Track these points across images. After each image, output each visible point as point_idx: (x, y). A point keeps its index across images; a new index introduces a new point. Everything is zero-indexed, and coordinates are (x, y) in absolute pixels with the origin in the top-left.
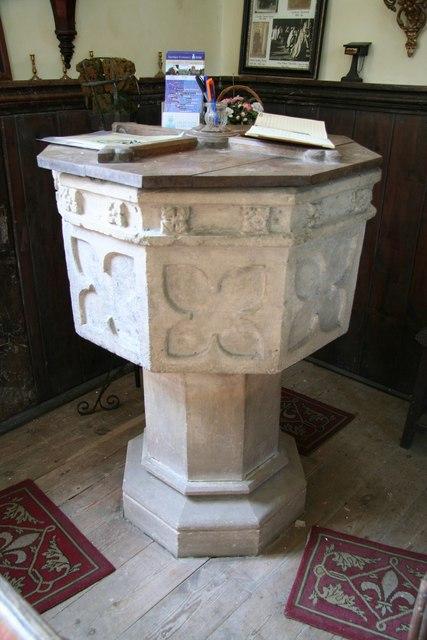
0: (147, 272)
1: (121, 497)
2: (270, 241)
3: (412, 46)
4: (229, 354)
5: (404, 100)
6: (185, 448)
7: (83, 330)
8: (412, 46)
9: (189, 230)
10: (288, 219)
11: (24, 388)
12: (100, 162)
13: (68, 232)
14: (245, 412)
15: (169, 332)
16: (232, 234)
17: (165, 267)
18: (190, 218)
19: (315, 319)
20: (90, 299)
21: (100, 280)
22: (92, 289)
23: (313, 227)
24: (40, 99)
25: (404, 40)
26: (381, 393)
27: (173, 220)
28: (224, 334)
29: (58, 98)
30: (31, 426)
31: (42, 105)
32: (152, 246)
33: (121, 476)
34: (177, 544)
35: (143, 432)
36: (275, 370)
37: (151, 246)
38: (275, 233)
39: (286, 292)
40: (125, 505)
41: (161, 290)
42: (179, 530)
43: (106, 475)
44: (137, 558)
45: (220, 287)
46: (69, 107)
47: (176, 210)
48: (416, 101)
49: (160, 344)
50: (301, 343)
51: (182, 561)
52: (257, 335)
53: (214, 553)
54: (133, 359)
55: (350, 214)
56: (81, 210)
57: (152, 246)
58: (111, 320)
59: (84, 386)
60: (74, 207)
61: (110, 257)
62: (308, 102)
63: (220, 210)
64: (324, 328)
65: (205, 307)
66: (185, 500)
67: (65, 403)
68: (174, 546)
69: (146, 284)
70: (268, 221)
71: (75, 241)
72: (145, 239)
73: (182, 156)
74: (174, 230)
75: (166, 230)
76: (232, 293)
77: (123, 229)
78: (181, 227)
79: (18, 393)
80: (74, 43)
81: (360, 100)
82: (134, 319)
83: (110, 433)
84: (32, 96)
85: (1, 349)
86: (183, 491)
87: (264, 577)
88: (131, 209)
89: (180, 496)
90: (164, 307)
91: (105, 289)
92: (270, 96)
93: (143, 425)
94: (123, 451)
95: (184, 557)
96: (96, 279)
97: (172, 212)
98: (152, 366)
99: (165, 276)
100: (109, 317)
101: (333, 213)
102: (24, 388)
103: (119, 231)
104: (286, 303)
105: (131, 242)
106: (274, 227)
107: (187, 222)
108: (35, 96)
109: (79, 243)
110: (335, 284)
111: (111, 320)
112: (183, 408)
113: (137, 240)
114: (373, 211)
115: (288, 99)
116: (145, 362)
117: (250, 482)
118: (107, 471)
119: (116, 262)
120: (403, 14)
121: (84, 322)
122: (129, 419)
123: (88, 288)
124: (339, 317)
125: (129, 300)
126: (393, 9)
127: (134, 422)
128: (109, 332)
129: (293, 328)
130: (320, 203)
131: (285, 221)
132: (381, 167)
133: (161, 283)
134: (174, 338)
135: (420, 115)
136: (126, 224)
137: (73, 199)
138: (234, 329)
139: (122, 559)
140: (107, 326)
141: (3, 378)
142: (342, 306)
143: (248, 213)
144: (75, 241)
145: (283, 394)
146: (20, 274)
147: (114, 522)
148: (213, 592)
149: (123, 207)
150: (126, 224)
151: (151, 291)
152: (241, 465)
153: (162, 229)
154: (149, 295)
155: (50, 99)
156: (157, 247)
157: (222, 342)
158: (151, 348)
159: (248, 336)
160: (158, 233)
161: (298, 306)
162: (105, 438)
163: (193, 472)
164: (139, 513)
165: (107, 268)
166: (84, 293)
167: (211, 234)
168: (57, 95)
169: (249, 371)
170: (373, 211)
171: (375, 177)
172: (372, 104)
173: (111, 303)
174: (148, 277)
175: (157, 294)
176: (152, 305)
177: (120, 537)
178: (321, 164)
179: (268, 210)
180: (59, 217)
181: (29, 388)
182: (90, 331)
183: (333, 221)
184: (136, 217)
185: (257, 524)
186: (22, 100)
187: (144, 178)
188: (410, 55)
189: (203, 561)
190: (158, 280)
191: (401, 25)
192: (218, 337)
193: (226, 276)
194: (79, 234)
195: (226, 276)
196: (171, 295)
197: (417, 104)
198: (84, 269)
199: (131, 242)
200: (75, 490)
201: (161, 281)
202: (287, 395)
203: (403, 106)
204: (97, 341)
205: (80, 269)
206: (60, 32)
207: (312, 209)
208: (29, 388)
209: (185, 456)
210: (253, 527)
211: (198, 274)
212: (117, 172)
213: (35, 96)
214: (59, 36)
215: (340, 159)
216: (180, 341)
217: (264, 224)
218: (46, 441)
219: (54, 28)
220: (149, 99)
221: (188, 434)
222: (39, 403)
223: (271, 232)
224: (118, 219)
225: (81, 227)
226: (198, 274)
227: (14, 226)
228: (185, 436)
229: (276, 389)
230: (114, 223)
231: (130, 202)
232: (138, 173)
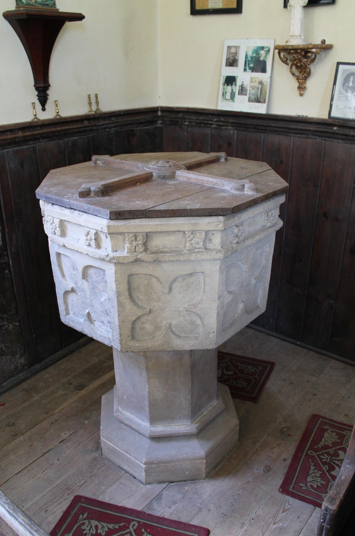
0: (116, 281)
1: (100, 439)
2: (206, 256)
3: (302, 88)
4: (179, 336)
5: (299, 127)
6: (147, 403)
7: (65, 319)
8: (302, 88)
9: (146, 250)
10: (219, 239)
11: (18, 356)
12: (105, 270)
13: (53, 249)
14: (192, 374)
15: (134, 323)
16: (178, 252)
17: (130, 276)
18: (146, 241)
19: (241, 306)
20: (72, 298)
21: (80, 284)
22: (73, 290)
23: (237, 243)
24: (24, 137)
25: (297, 84)
26: (292, 345)
27: (134, 244)
28: (174, 322)
29: (37, 134)
30: (25, 385)
31: (25, 140)
32: (118, 263)
33: (98, 424)
34: (144, 474)
35: (113, 388)
36: (213, 346)
37: (119, 263)
38: (209, 249)
39: (219, 291)
40: (102, 445)
41: (127, 294)
42: (145, 464)
43: (86, 422)
44: (114, 486)
45: (170, 289)
46: (45, 140)
47: (136, 237)
48: (308, 128)
49: (127, 331)
50: (232, 325)
51: (148, 486)
52: (199, 322)
53: (173, 480)
54: (107, 342)
55: (264, 229)
56: (63, 234)
57: (118, 263)
58: (89, 314)
59: (61, 353)
60: (58, 231)
61: (87, 268)
62: (228, 126)
63: (168, 235)
64: (247, 311)
65: (160, 304)
66: (149, 441)
67: (49, 366)
68: (142, 476)
69: (115, 289)
70: (204, 242)
71: (58, 255)
72: (114, 258)
73: (140, 188)
74: (135, 251)
75: (130, 251)
76: (180, 293)
77: (97, 251)
78: (140, 248)
79: (13, 360)
80: (48, 92)
81: (267, 126)
82: (107, 313)
83: (87, 388)
84: (17, 135)
85: (1, 326)
86: (147, 435)
87: (210, 495)
88: (103, 236)
89: (145, 438)
90: (128, 305)
91: (83, 290)
92: (197, 121)
93: (112, 382)
94: (98, 403)
95: (150, 484)
96: (76, 283)
97: (133, 238)
98: (122, 348)
99: (129, 283)
100: (87, 311)
101: (251, 229)
102: (18, 356)
103: (93, 250)
104: (219, 298)
105: (103, 260)
106: (209, 245)
107: (145, 244)
108: (20, 134)
109: (62, 257)
110: (255, 279)
111: (89, 314)
112: (144, 374)
113: (108, 259)
114: (280, 224)
115: (212, 124)
116: (116, 345)
117: (197, 425)
118: (86, 418)
119: (91, 272)
120: (294, 68)
121: (68, 314)
122: (100, 376)
123: (70, 289)
124: (259, 302)
125: (102, 299)
126: (287, 64)
127: (105, 378)
128: (88, 322)
129: (225, 315)
130: (242, 224)
131: (217, 240)
132: (286, 193)
133: (127, 288)
134: (138, 326)
135: (311, 138)
136: (98, 246)
137: (58, 225)
138: (182, 318)
139: (103, 488)
140: (86, 318)
141: (1, 349)
142: (260, 293)
143: (189, 237)
144: (58, 255)
145: (218, 356)
146: (12, 269)
147: (95, 459)
148: (173, 508)
149: (96, 234)
150: (98, 246)
151: (119, 294)
152: (190, 413)
153: (126, 251)
154: (117, 298)
155: (31, 136)
156: (122, 264)
157: (174, 329)
158: (121, 335)
159: (193, 323)
160: (124, 253)
161: (228, 298)
162: (83, 392)
163: (153, 420)
164: (113, 451)
165: (85, 275)
166: (66, 293)
167: (162, 252)
168: (35, 132)
169: (194, 348)
170: (280, 224)
171: (282, 199)
172: (275, 129)
173: (89, 301)
174: (116, 285)
175: (123, 297)
176: (120, 304)
177: (100, 471)
178: (242, 193)
179: (204, 234)
180: (46, 237)
181: (22, 356)
182: (73, 321)
183: (252, 236)
184: (107, 243)
185: (204, 456)
186: (10, 139)
187: (111, 213)
188: (301, 95)
189: (164, 485)
190: (124, 286)
191: (293, 74)
192: (170, 325)
193: (175, 280)
194: (61, 251)
195: (175, 280)
196: (135, 295)
197: (309, 130)
198: (66, 276)
199: (103, 260)
200: (64, 435)
201: (126, 287)
202: (219, 352)
203: (298, 132)
204: (78, 328)
205: (63, 275)
206: (38, 85)
207: (236, 230)
208: (22, 356)
209: (147, 409)
210: (200, 458)
211: (154, 281)
212: (92, 206)
213: (20, 134)
214: (37, 88)
215: (257, 190)
216: (142, 329)
217: (202, 243)
218: (37, 397)
219: (33, 83)
220: (106, 128)
221: (149, 392)
222: (29, 367)
223: (206, 249)
224: (93, 243)
225: (64, 246)
226: (154, 281)
227: (6, 233)
228: (147, 394)
229: (215, 355)
230: (89, 245)
231: (102, 232)
232: (108, 208)
